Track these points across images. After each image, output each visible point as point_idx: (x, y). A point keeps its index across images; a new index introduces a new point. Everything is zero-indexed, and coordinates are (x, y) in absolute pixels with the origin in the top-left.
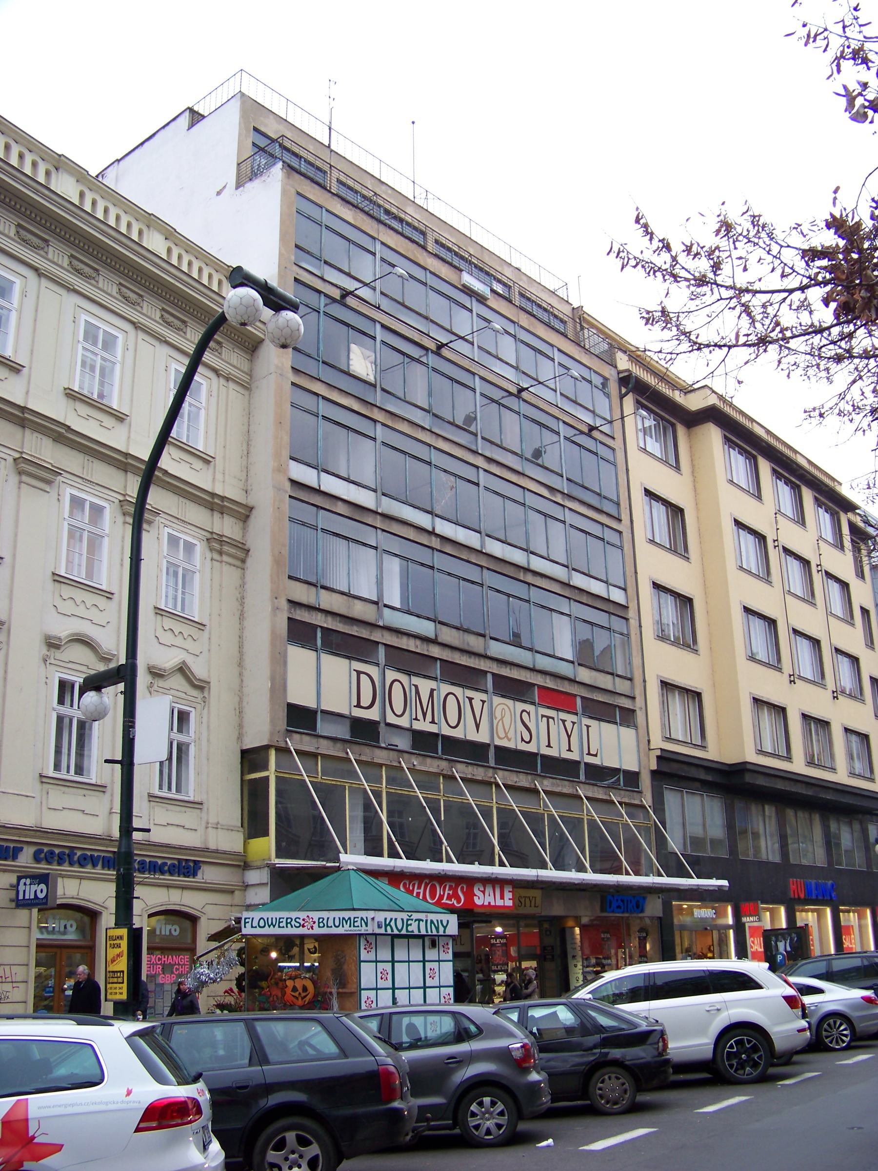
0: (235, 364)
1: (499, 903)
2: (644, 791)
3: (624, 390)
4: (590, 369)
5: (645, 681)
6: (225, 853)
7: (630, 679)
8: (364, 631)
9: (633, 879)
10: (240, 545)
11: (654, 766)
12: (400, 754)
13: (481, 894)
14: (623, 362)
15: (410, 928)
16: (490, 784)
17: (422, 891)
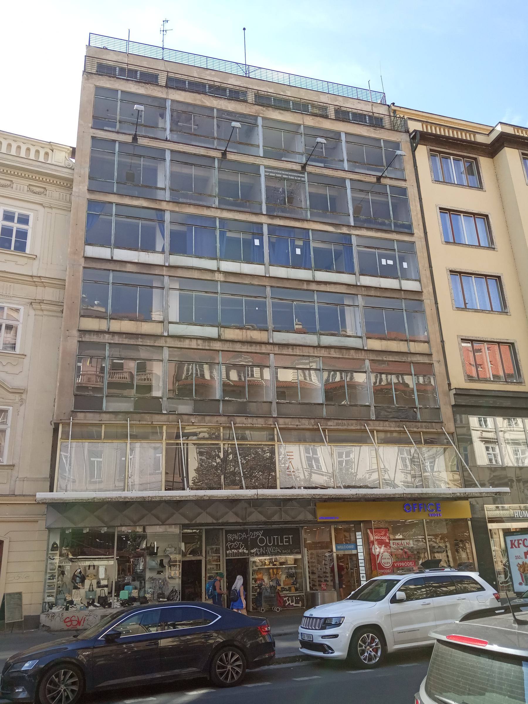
2: (445, 422)
5: (442, 341)
7: (428, 342)
8: (148, 341)
12: (178, 416)
14: (413, 126)
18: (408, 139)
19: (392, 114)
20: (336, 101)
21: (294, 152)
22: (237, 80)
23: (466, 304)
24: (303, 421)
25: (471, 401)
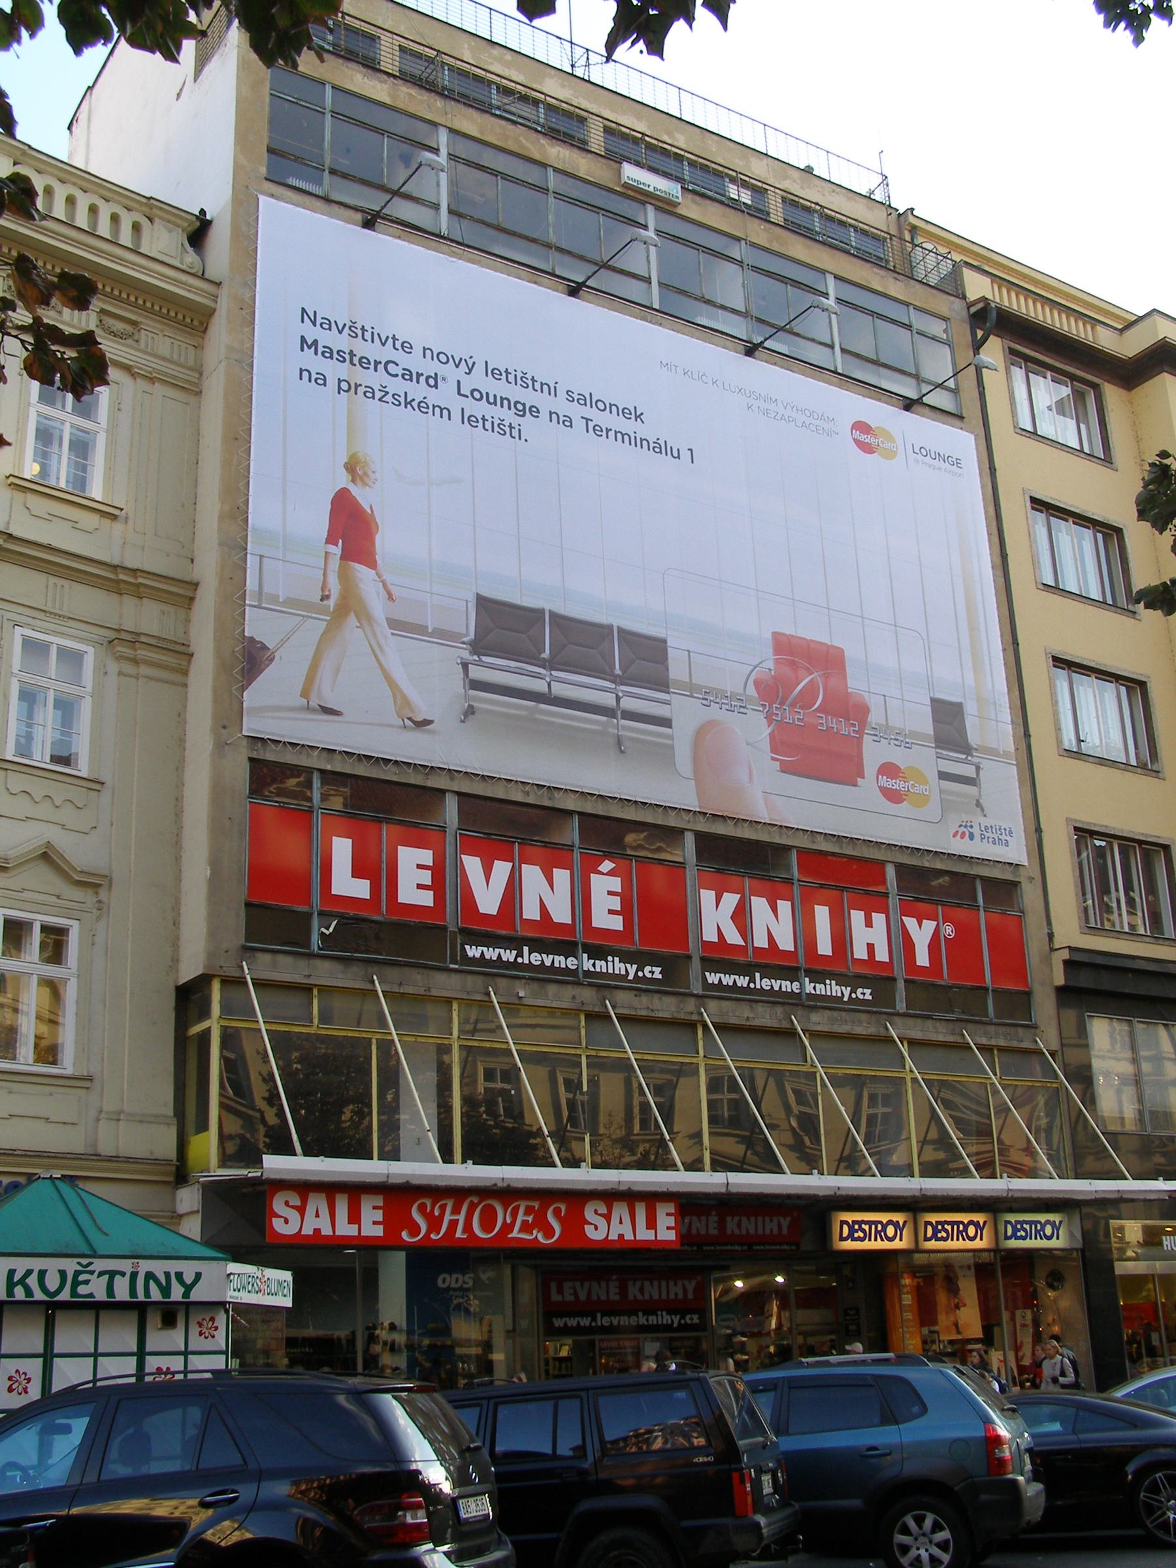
0: (167, 354)
1: (645, 1234)
3: (980, 333)
4: (907, 304)
6: (128, 1160)
9: (788, 1181)
10: (178, 648)
11: (1060, 980)
13: (601, 1222)
14: (977, 287)
15: (82, 1290)
16: (691, 1026)
17: (461, 1218)
18: (965, 313)
19: (908, 237)
20: (785, 178)
21: (708, 302)
22: (563, 86)
23: (1080, 741)
24: (760, 1008)
25: (1107, 983)
